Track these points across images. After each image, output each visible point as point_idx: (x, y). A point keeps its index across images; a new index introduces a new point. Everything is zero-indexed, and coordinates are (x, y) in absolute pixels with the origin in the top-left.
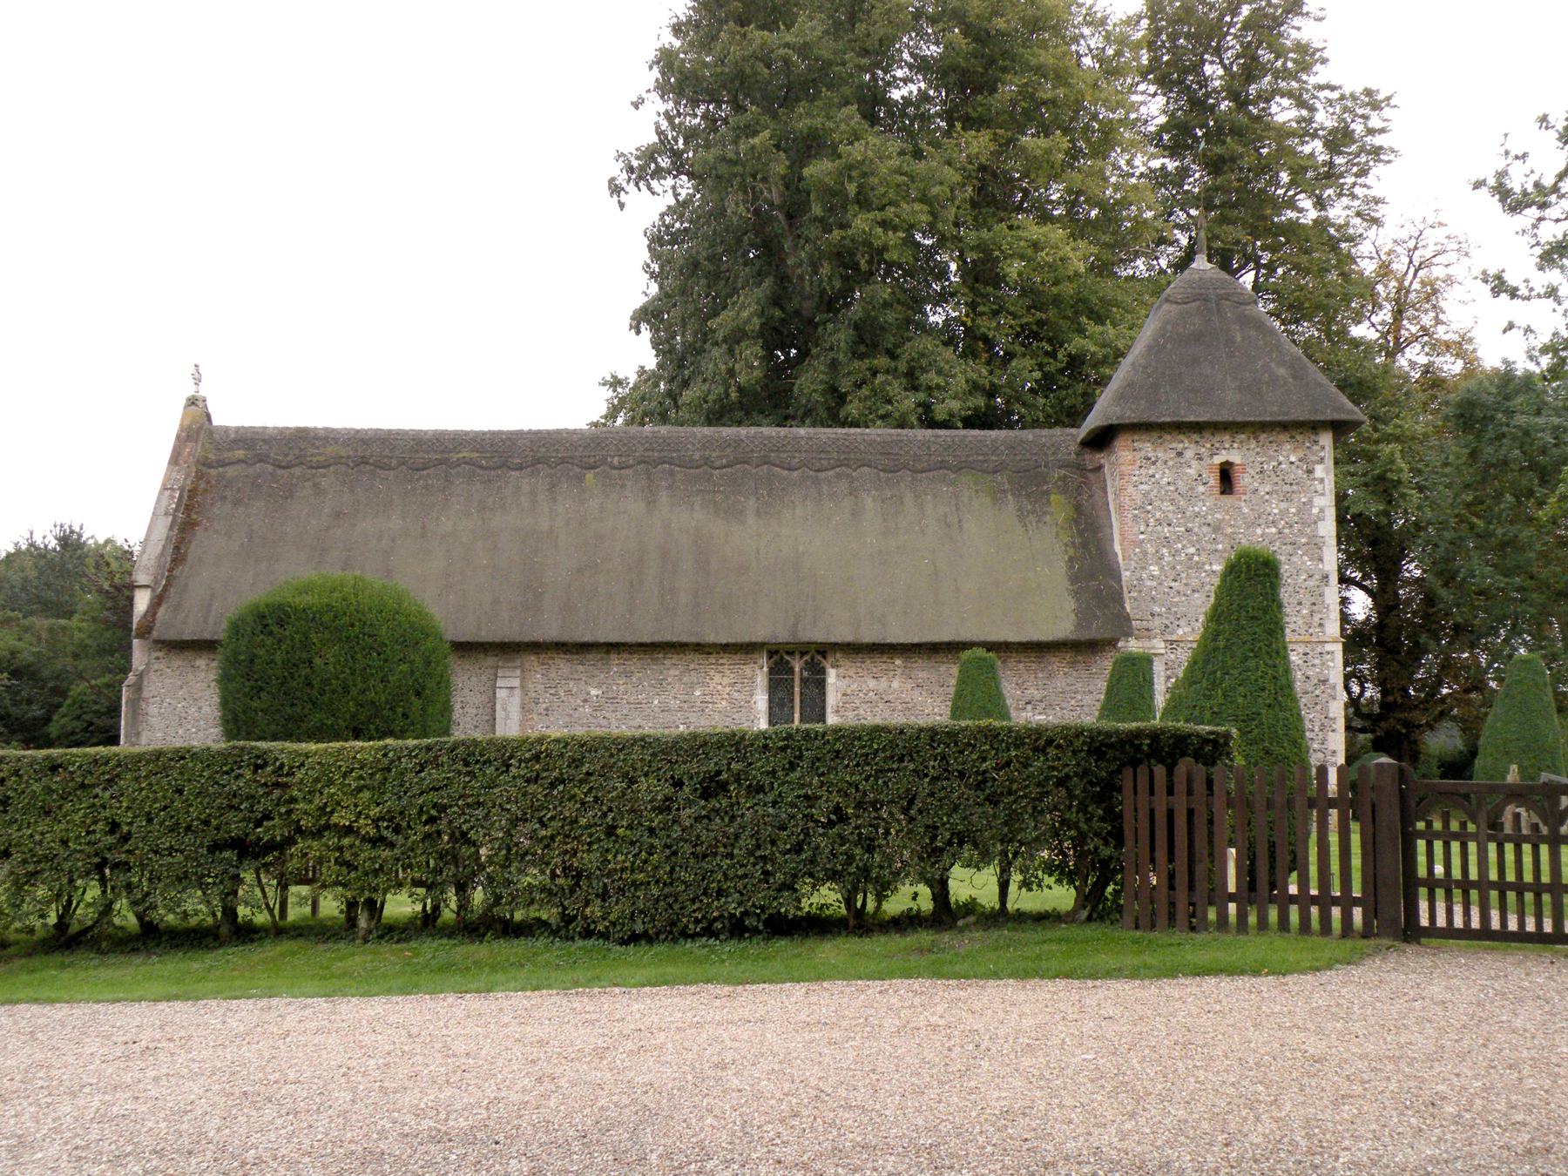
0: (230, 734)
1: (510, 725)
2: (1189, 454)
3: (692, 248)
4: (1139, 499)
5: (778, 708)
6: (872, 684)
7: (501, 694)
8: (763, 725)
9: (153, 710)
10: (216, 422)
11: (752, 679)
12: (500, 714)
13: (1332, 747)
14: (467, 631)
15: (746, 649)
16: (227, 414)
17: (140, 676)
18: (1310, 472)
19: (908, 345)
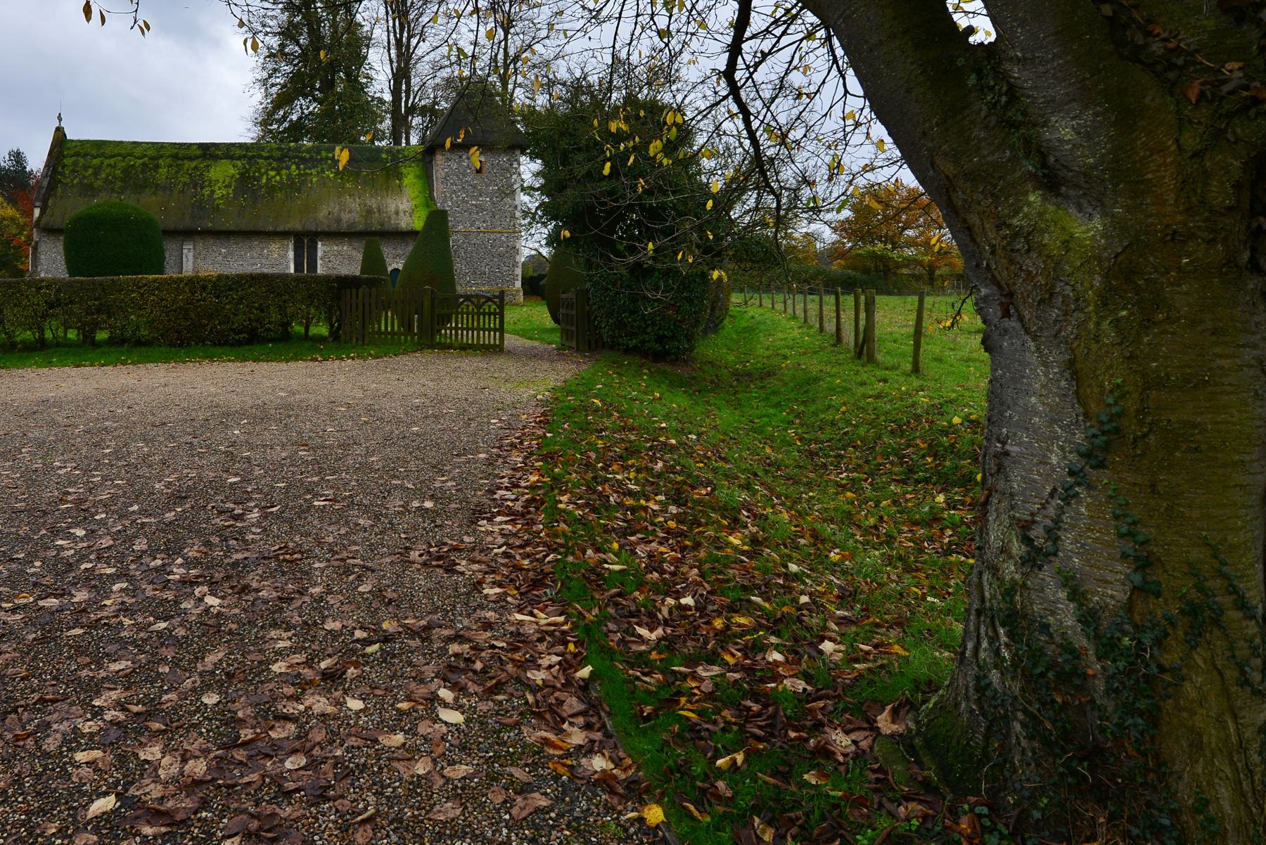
0: (72, 274)
1: (188, 268)
2: (464, 157)
3: (352, 127)
4: (443, 174)
5: (298, 266)
6: (336, 248)
7: (185, 251)
8: (292, 271)
9: (42, 257)
10: (69, 138)
11: (288, 245)
12: (184, 259)
13: (516, 273)
14: (171, 225)
15: (284, 235)
16: (74, 133)
17: (37, 243)
18: (511, 165)
19: (1032, 345)
